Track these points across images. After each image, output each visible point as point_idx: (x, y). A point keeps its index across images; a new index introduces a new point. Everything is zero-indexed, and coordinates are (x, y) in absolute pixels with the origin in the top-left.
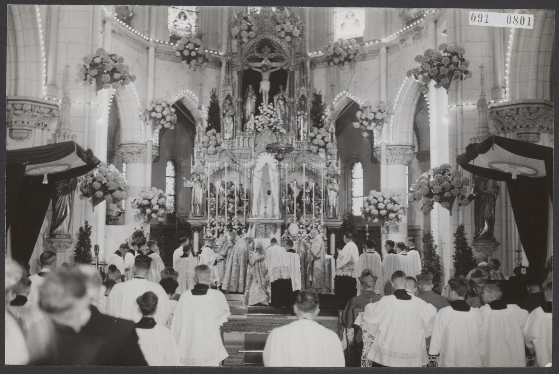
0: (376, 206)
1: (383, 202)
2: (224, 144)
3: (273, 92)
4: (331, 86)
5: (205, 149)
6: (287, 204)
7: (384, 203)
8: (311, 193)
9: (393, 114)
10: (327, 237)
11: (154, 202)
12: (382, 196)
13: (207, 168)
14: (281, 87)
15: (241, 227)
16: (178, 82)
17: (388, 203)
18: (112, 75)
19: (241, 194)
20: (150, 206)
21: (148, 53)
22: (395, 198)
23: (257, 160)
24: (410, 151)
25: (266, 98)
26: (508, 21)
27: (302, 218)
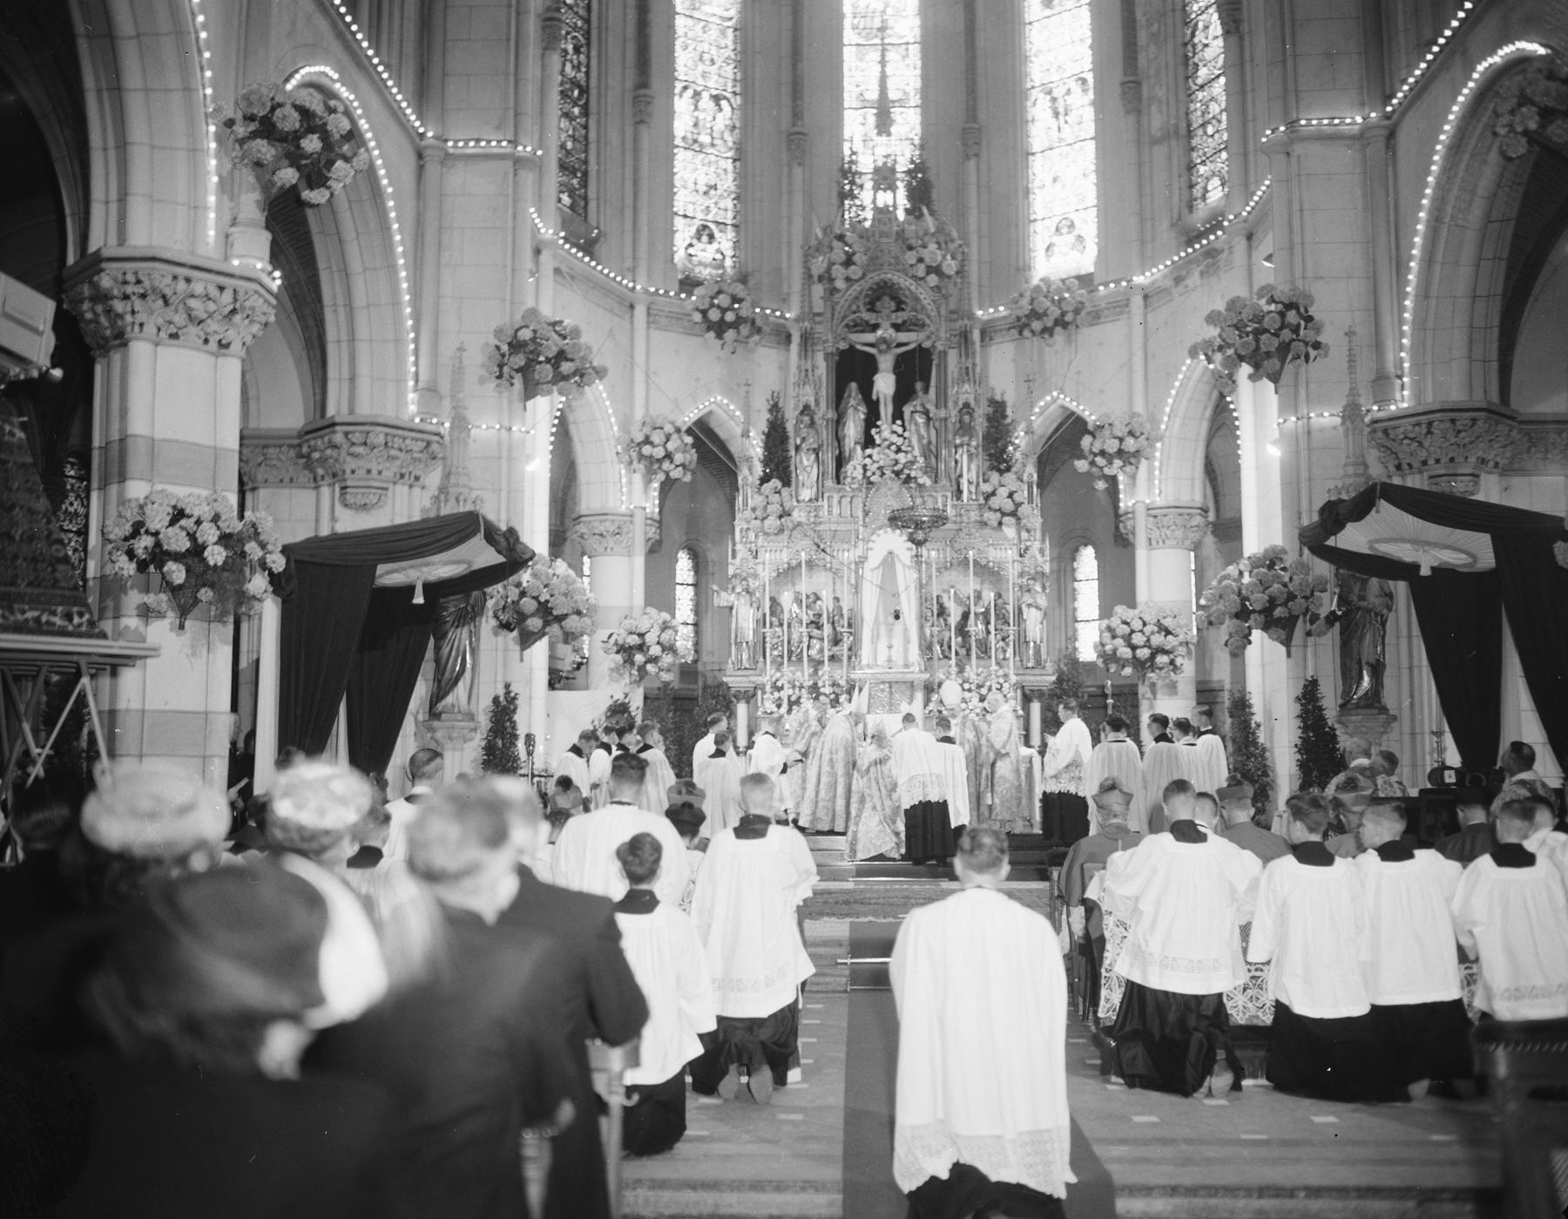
0: (1127, 639)
1: (1141, 631)
3: (903, 395)
6: (935, 639)
9: (1160, 439)
11: (651, 638)
14: (919, 386)
16: (698, 379)
18: (556, 366)
20: (641, 648)
22: (1167, 622)
23: (871, 545)
24: (1198, 520)
25: (886, 410)
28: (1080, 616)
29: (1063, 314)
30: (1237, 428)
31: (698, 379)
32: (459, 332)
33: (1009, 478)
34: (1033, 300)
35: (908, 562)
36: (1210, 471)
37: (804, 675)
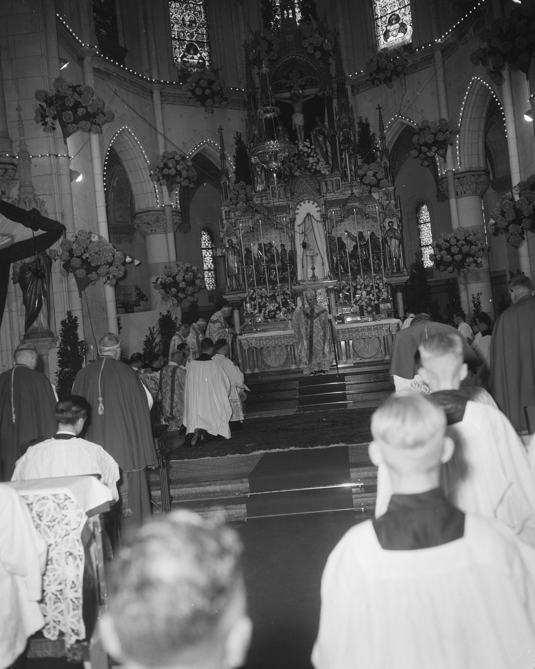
0: (448, 250)
1: (456, 245)
3: (308, 127)
4: (377, 109)
5: (233, 206)
7: (458, 246)
8: (366, 245)
9: (458, 132)
10: (392, 297)
11: (179, 278)
12: (455, 238)
13: (239, 229)
14: (318, 119)
15: (286, 297)
16: (195, 130)
17: (463, 245)
18: (75, 113)
20: (175, 284)
21: (152, 98)
22: (471, 238)
23: (297, 211)
24: (483, 178)
25: (301, 135)
28: (423, 244)
29: (396, 67)
30: (504, 116)
31: (195, 130)
32: (19, 100)
33: (373, 165)
34: (378, 62)
35: (319, 219)
36: (488, 153)
37: (266, 291)
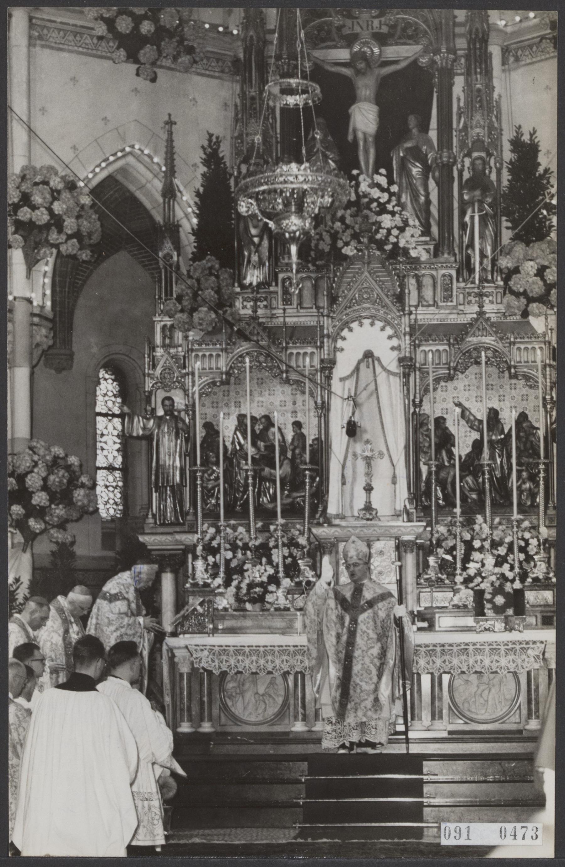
2: (245, 300)
6: (163, 300)
13: (193, 374)
14: (412, 121)
15: (295, 551)
16: (105, 119)
19: (297, 451)
26: (501, 836)
27: (479, 518)
